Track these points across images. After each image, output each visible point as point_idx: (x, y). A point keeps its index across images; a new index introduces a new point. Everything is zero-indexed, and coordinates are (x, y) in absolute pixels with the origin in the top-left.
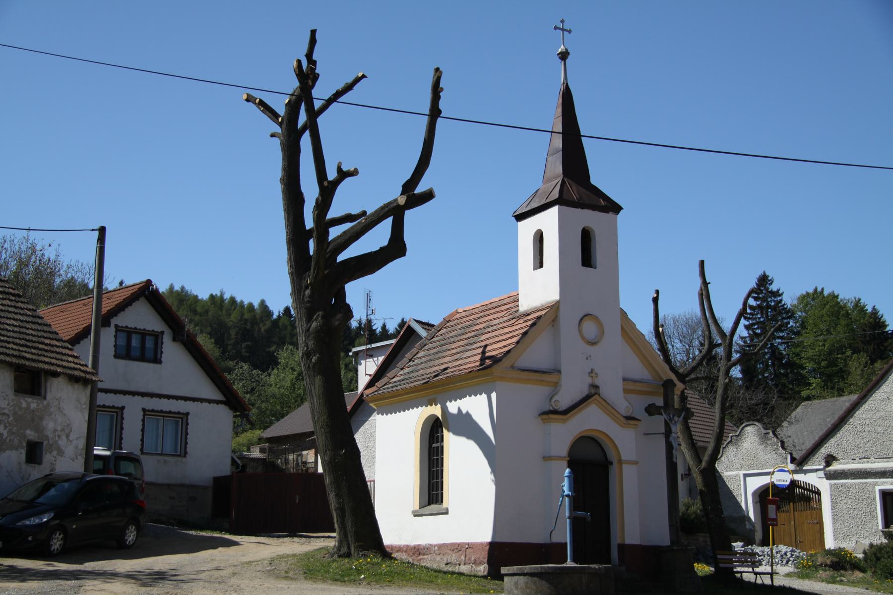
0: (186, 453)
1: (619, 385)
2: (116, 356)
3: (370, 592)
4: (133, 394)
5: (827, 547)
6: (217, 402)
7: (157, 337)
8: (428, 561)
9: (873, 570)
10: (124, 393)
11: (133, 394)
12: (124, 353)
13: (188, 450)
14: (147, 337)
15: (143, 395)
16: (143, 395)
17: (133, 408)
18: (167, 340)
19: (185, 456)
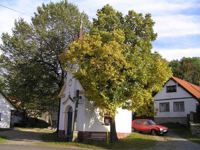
0: (184, 110)
1: (31, 22)
2: (166, 92)
3: (76, 148)
4: (171, 99)
5: (9, 127)
6: (191, 98)
7: (175, 86)
8: (93, 136)
9: (67, 5)
10: (169, 99)
11: (171, 99)
12: (168, 91)
13: (185, 110)
14: (171, 88)
15: (173, 99)
16: (173, 99)
17: (171, 103)
18: (177, 86)
19: (184, 111)
